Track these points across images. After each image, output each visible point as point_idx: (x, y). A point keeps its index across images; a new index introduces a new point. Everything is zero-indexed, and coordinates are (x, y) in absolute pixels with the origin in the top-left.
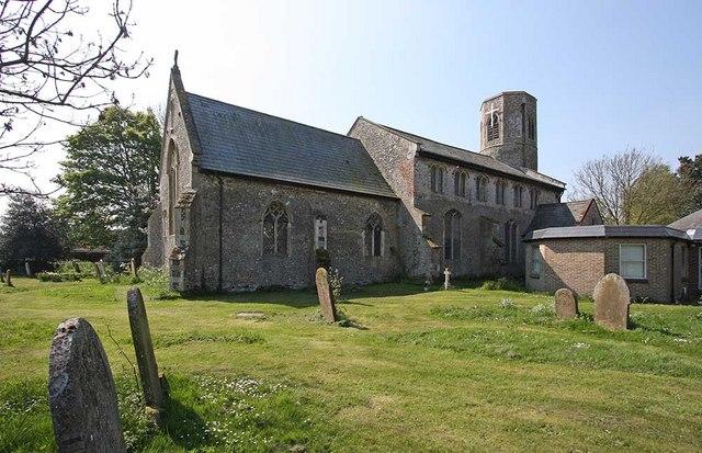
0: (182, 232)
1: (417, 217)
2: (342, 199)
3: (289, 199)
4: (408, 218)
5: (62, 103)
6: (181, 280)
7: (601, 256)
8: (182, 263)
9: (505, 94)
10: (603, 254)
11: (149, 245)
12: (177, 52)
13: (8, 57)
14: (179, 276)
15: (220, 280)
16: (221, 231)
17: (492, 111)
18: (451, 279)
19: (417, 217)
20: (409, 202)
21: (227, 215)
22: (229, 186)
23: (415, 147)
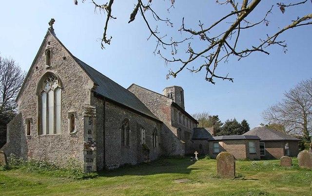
0: (90, 132)
1: (174, 131)
2: (146, 119)
3: (131, 117)
4: (167, 130)
5: (273, 42)
6: (94, 164)
7: (244, 146)
8: (94, 153)
9: (175, 87)
10: (244, 146)
11: (8, 141)
12: (116, 18)
13: (310, 116)
14: (92, 160)
15: (104, 162)
16: (104, 133)
17: (170, 92)
18: (198, 156)
19: (174, 131)
20: (169, 124)
21: (107, 124)
22: (109, 107)
23: (90, 85)
